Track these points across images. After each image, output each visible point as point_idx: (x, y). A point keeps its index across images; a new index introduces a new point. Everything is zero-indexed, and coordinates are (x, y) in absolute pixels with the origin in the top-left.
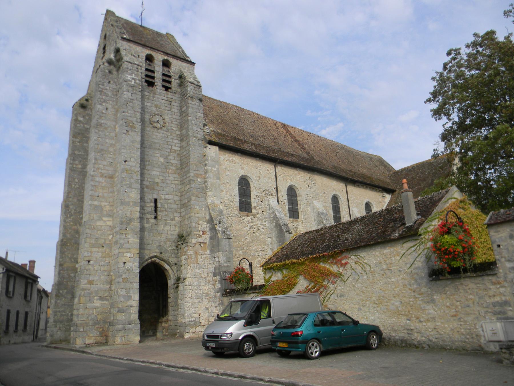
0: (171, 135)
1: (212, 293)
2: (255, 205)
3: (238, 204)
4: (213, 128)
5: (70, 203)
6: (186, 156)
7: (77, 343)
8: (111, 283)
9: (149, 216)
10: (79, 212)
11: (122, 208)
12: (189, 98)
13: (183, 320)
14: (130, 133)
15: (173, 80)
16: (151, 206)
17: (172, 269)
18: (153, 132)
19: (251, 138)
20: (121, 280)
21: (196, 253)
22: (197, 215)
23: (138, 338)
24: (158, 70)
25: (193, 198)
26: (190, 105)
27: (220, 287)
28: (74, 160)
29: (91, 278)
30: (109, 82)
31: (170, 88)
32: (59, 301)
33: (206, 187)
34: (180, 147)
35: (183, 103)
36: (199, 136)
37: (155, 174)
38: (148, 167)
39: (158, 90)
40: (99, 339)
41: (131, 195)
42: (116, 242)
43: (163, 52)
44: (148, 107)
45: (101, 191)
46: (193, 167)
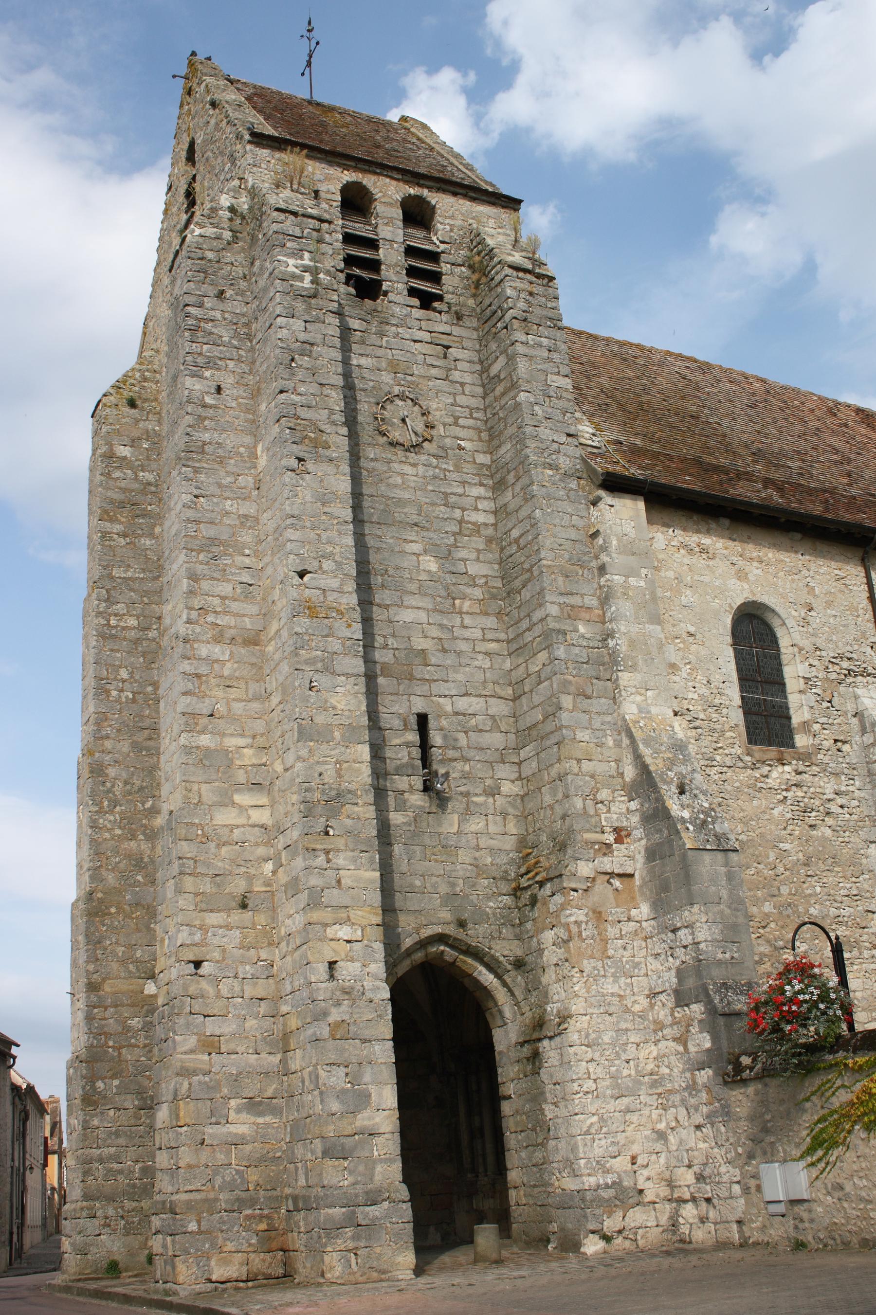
0: (458, 469)
1: (676, 1073)
2: (807, 716)
3: (737, 717)
4: (612, 432)
5: (108, 758)
6: (522, 542)
7: (181, 1279)
8: (284, 1044)
9: (401, 782)
10: (141, 789)
11: (304, 753)
12: (516, 324)
13: (570, 1184)
14: (310, 466)
15: (445, 268)
16: (408, 745)
17: (505, 984)
18: (389, 462)
19: (756, 462)
20: (817, 412)
21: (598, 916)
22: (586, 766)
23: (408, 1258)
24: (389, 237)
25: (567, 701)
26: (520, 348)
27: (708, 1045)
28: (109, 600)
29: (211, 1027)
30: (222, 292)
31: (440, 298)
32: (96, 1122)
33: (613, 654)
34: (495, 513)
35: (493, 346)
36: (565, 463)
37: (410, 617)
38: (381, 596)
39: (397, 309)
40: (259, 1262)
41: (333, 701)
42: (293, 887)
43: (404, 172)
44: (366, 374)
45: (219, 693)
46: (553, 582)
